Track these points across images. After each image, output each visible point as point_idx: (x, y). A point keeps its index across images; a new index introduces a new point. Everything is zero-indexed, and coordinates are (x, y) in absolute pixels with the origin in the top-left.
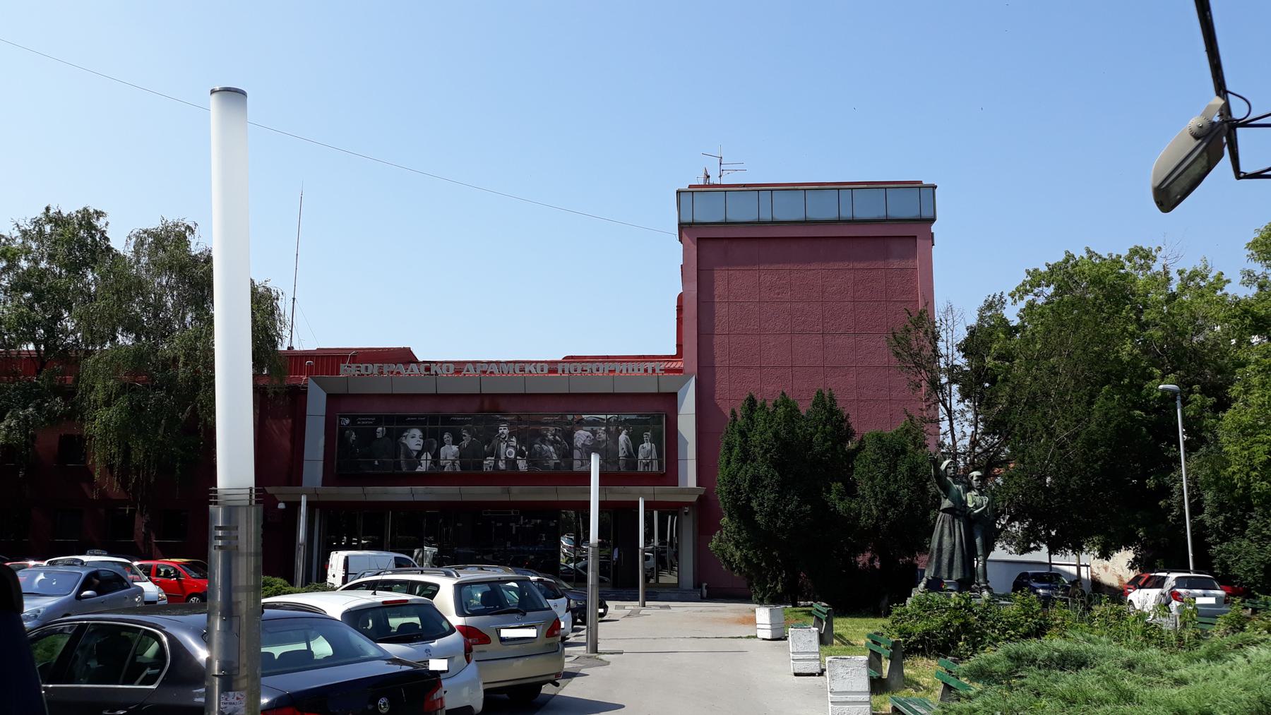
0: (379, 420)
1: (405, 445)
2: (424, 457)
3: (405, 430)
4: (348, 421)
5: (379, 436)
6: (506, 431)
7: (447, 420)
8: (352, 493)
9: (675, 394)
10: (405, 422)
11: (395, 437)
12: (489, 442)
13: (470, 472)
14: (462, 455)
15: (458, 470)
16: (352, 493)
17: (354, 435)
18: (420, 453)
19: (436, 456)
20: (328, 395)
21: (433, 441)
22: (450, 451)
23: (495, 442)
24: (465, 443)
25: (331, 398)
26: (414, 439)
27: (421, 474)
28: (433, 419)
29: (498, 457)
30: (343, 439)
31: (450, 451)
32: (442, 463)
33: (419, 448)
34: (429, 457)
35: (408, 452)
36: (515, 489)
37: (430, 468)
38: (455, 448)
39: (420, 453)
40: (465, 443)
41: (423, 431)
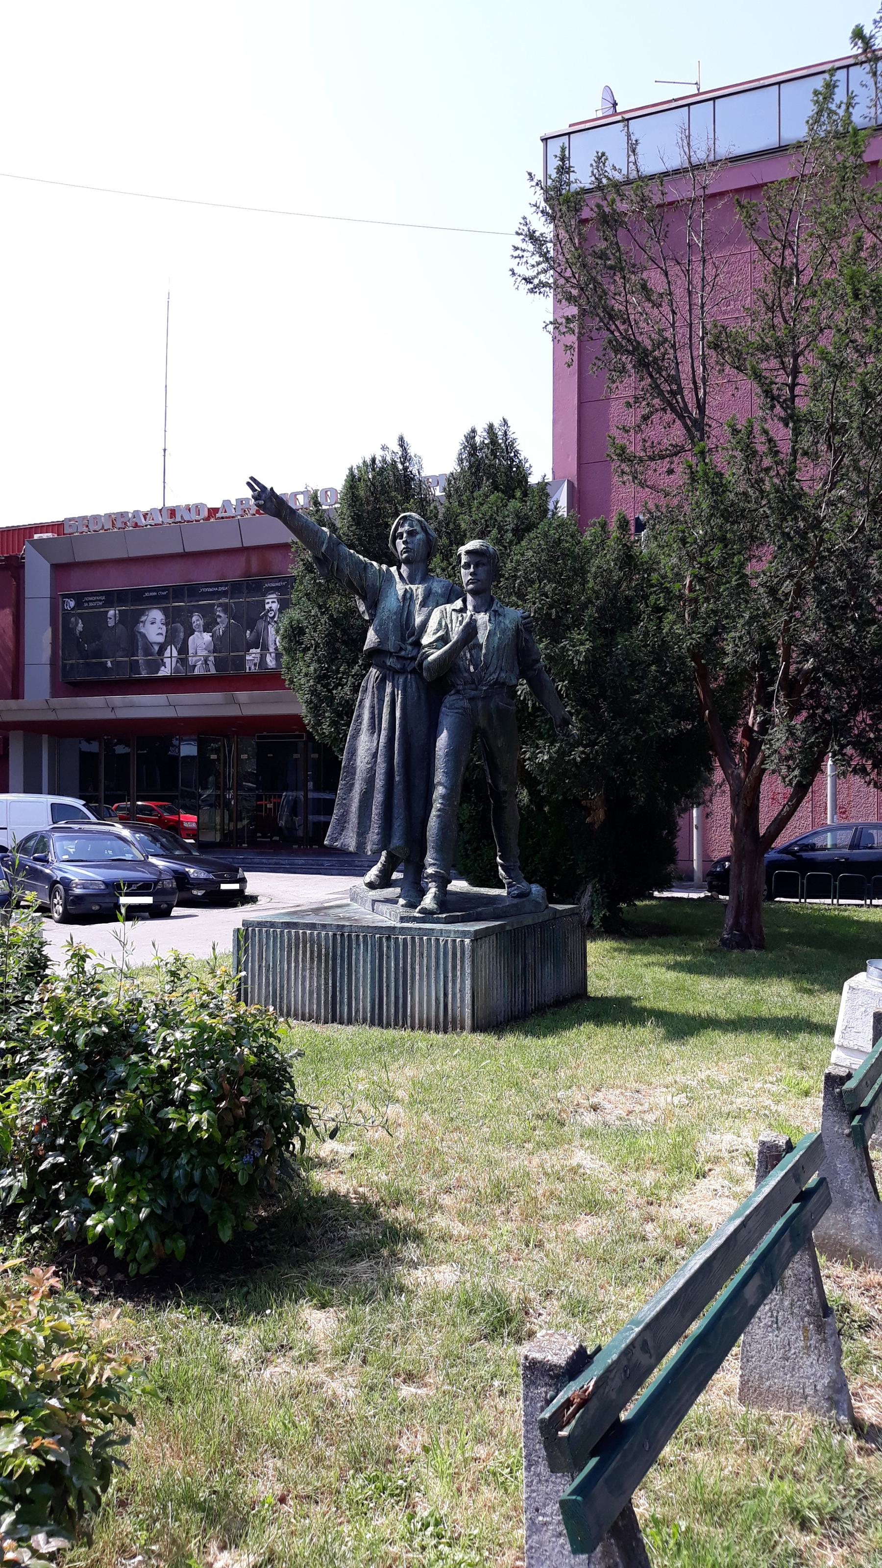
0: (112, 598)
1: (144, 636)
2: (167, 653)
3: (142, 612)
4: (72, 604)
5: (111, 623)
6: (275, 606)
7: (192, 591)
8: (96, 707)
9: (209, 509)
10: (137, 600)
11: (131, 620)
12: (251, 626)
13: (228, 675)
14: (217, 647)
15: (213, 671)
16: (96, 707)
17: (80, 626)
18: (162, 648)
19: (183, 650)
20: (52, 565)
21: (179, 633)
22: (201, 642)
23: (261, 625)
24: (220, 629)
25: (58, 569)
26: (154, 626)
27: (165, 679)
28: (177, 592)
29: (265, 648)
30: (68, 631)
31: (201, 642)
32: (191, 660)
33: (161, 639)
34: (175, 653)
35: (148, 646)
36: (242, 696)
37: (177, 670)
38: (207, 637)
39: (162, 648)
40: (220, 629)
41: (165, 611)
